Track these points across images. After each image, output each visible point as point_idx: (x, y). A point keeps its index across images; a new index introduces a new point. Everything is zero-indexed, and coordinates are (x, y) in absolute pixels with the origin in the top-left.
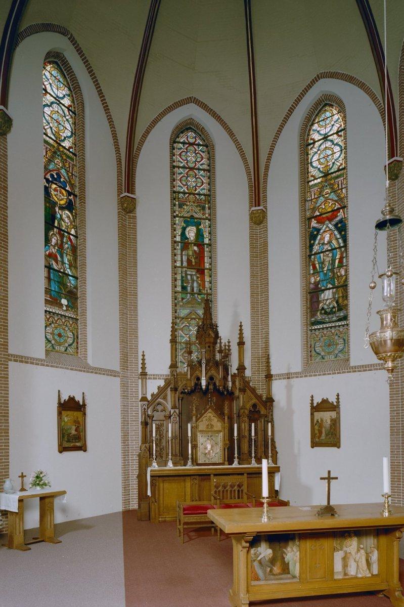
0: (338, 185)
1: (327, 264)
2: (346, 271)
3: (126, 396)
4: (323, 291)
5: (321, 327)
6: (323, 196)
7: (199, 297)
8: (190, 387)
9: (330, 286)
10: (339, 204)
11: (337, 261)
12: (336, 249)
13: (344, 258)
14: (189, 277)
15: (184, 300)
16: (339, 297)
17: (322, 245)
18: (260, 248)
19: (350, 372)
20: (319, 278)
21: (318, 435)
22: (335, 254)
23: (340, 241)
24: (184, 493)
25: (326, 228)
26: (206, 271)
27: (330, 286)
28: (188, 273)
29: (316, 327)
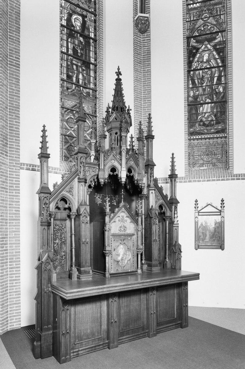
0: (217, 11)
1: (206, 80)
2: (225, 89)
3: (5, 188)
4: (202, 104)
5: (200, 137)
6: (202, 19)
7: (85, 90)
8: (103, 179)
9: (208, 100)
10: (219, 29)
11: (215, 79)
12: (214, 67)
13: (222, 76)
14: (75, 67)
15: (70, 90)
16: (217, 112)
17: (201, 63)
18: (143, 55)
19: (234, 179)
20: (198, 92)
21: (202, 237)
22: (214, 73)
23: (219, 61)
24: (99, 315)
25: (205, 48)
26: (91, 65)
27: (208, 100)
28: (74, 62)
29: (195, 137)
